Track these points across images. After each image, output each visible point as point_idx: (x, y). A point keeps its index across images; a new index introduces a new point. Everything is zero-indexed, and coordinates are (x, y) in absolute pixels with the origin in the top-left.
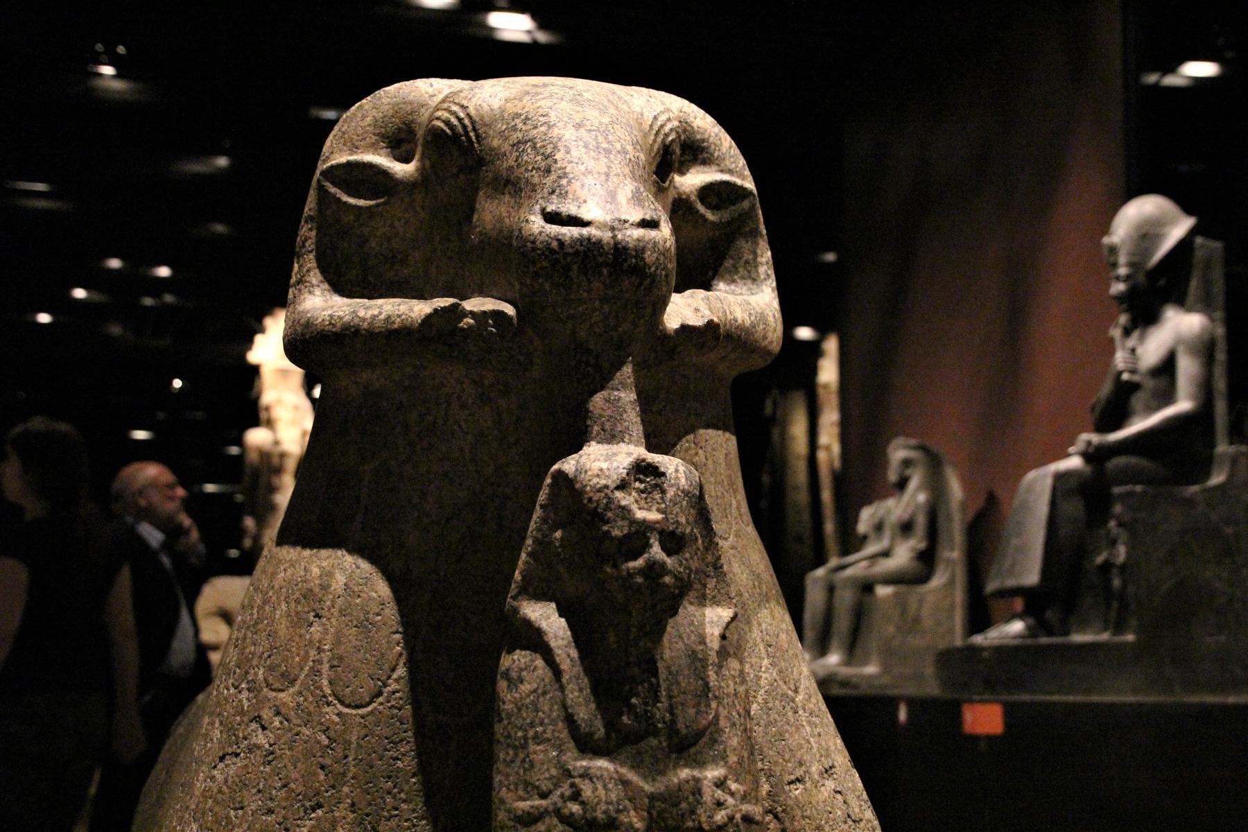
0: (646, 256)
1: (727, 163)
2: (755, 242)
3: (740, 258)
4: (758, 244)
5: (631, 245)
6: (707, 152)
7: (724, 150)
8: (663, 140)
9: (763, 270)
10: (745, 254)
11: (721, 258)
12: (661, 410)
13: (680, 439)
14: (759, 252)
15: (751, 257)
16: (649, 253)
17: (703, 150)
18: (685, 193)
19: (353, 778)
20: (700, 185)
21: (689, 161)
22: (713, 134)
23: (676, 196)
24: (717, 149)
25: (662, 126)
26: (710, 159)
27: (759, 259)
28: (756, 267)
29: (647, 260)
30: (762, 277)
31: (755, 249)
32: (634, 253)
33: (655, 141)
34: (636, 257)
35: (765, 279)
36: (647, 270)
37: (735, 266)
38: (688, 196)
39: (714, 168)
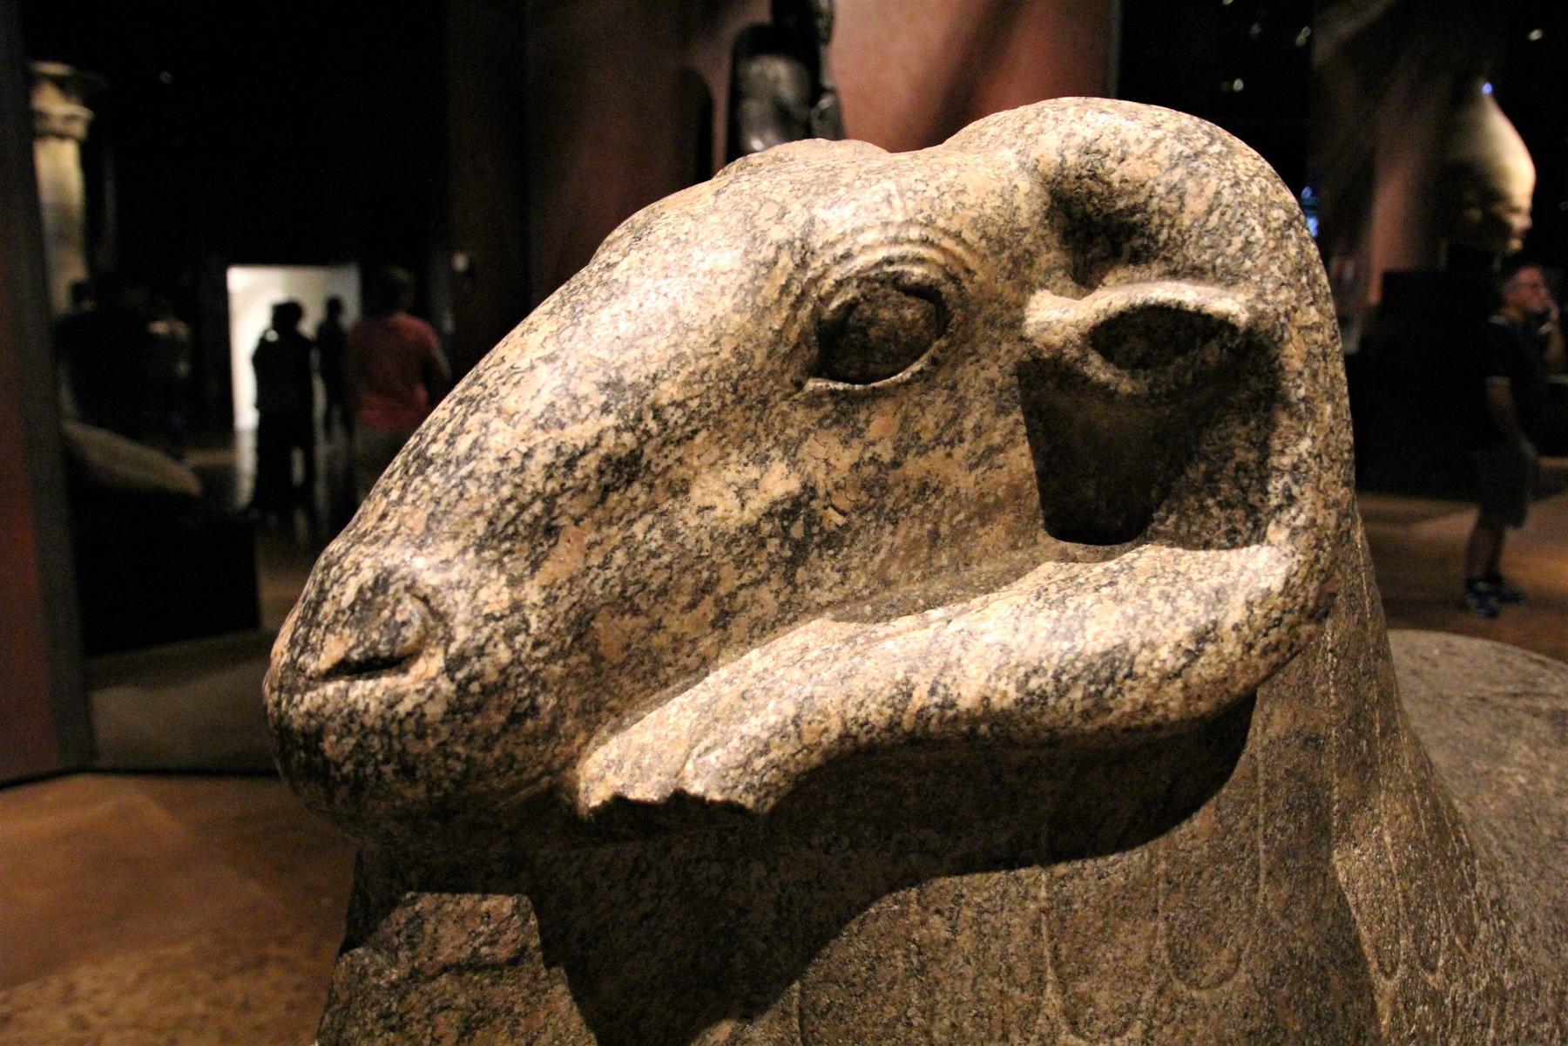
0: (326, 745)
1: (1192, 252)
2: (1267, 421)
3: (1226, 460)
4: (1275, 426)
5: (295, 725)
6: (1143, 235)
7: (1187, 222)
8: (816, 313)
9: (1280, 485)
10: (1237, 451)
11: (1183, 458)
12: (829, 845)
13: (875, 896)
14: (1276, 444)
15: (1252, 456)
16: (333, 738)
17: (1132, 230)
18: (1048, 346)
19: (1243, 859)
20: (1091, 322)
21: (1104, 259)
22: (1160, 190)
23: (1026, 357)
24: (1168, 222)
25: (814, 281)
26: (1147, 248)
27: (1274, 461)
28: (1263, 480)
29: (329, 753)
30: (1274, 502)
31: (1267, 438)
32: (301, 741)
33: (790, 321)
34: (306, 748)
35: (1279, 508)
36: (333, 772)
37: (1209, 478)
38: (1059, 352)
39: (1157, 268)
